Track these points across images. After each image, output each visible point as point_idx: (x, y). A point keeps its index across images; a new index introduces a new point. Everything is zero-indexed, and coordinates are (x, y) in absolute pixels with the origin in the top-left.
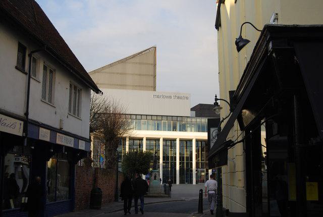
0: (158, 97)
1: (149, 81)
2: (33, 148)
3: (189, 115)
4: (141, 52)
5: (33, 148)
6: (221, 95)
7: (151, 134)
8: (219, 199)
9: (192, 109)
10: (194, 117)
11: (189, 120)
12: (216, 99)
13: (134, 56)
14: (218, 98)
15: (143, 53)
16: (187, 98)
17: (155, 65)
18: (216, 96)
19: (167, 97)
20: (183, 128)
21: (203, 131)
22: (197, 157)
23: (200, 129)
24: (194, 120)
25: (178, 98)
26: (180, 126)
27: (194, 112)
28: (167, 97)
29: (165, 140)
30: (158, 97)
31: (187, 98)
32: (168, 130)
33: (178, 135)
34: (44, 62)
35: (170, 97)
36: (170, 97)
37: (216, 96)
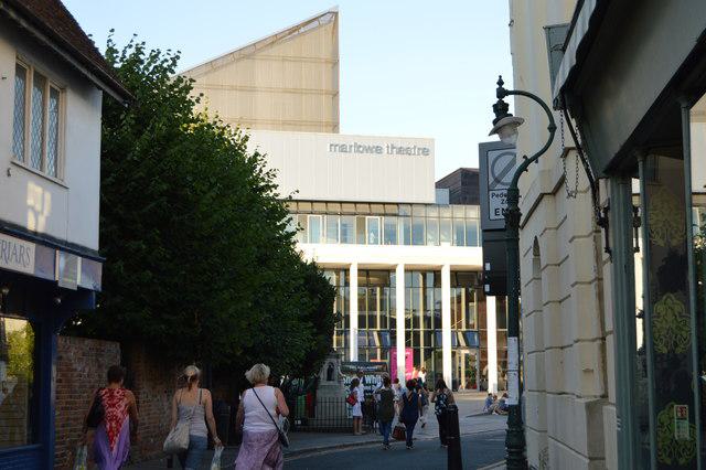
0: (343, 149)
1: (320, 107)
2: (6, 291)
3: (432, 200)
4: (297, 28)
5: (6, 291)
6: (518, 76)
7: (609, 277)
8: (514, 441)
9: (439, 185)
10: (445, 206)
11: (433, 213)
12: (502, 93)
13: (276, 39)
14: (508, 86)
15: (302, 30)
16: (425, 152)
17: (335, 63)
18: (500, 83)
19: (369, 149)
20: (415, 237)
21: (471, 243)
22: (455, 317)
23: (462, 239)
24: (447, 213)
25: (400, 151)
26: (406, 231)
27: (446, 192)
28: (369, 149)
29: (365, 272)
30: (343, 149)
31: (425, 152)
32: (359, 243)
33: (399, 256)
34: (17, 58)
35: (378, 150)
36: (378, 150)
37: (500, 83)
